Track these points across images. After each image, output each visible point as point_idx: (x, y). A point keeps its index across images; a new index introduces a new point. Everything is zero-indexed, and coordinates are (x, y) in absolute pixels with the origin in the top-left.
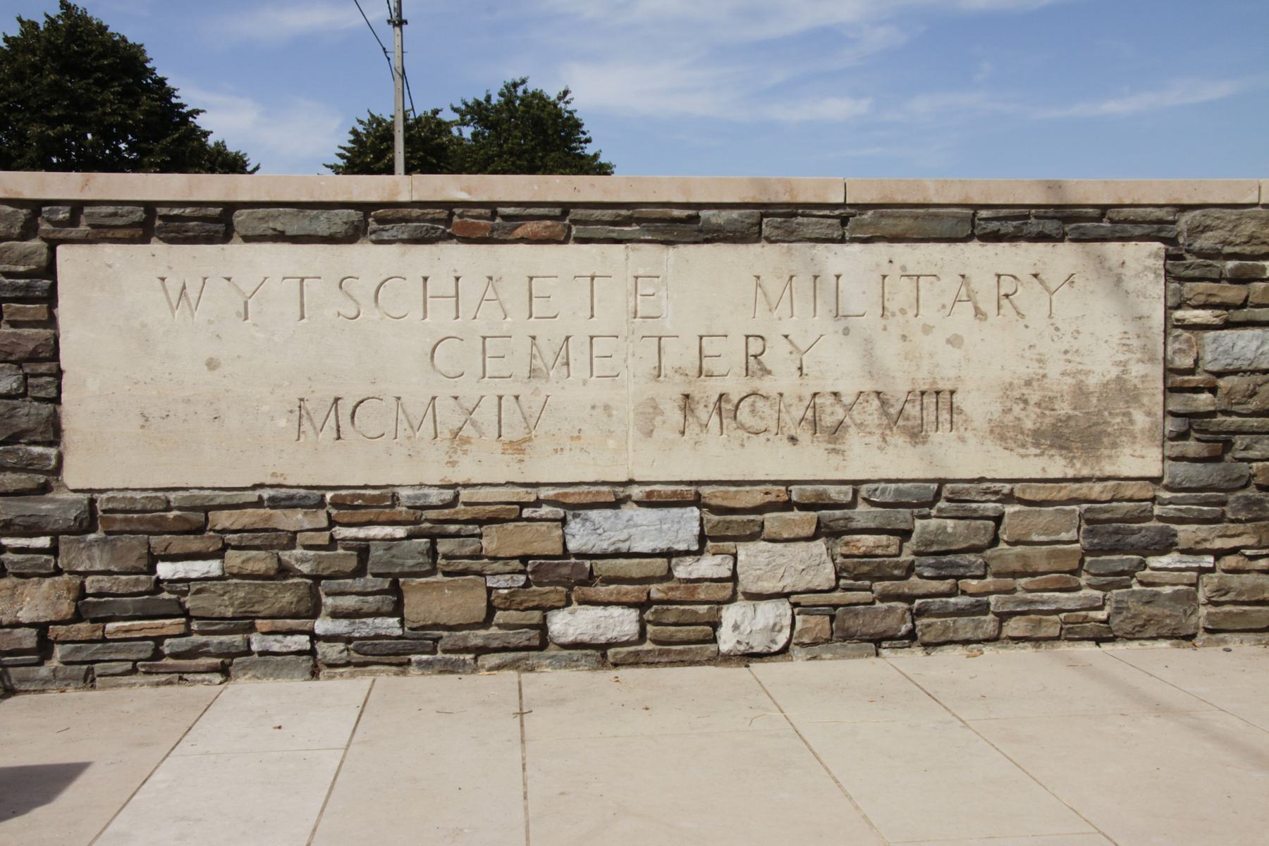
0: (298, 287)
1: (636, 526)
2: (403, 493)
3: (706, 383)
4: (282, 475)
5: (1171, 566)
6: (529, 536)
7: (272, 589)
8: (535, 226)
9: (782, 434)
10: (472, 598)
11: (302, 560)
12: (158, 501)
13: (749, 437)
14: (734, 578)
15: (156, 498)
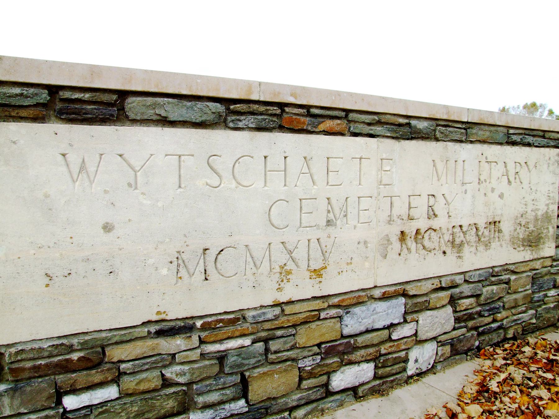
0: (177, 163)
1: (377, 313)
2: (250, 314)
3: (411, 224)
4: (165, 312)
5: (554, 295)
6: (324, 330)
7: (158, 400)
8: (332, 123)
9: (441, 250)
10: (290, 377)
11: (183, 374)
12: (63, 347)
13: (427, 254)
14: (416, 334)
15: (62, 344)
